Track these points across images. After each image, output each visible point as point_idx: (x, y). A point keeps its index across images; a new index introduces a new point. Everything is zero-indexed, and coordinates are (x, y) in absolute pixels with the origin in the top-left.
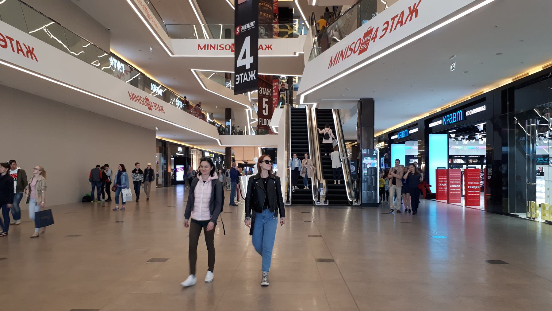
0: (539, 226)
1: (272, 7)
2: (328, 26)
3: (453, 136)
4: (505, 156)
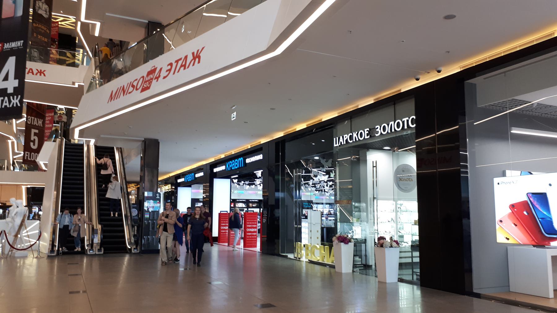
0: (304, 265)
1: (50, 30)
2: (110, 60)
3: (235, 181)
4: (277, 200)
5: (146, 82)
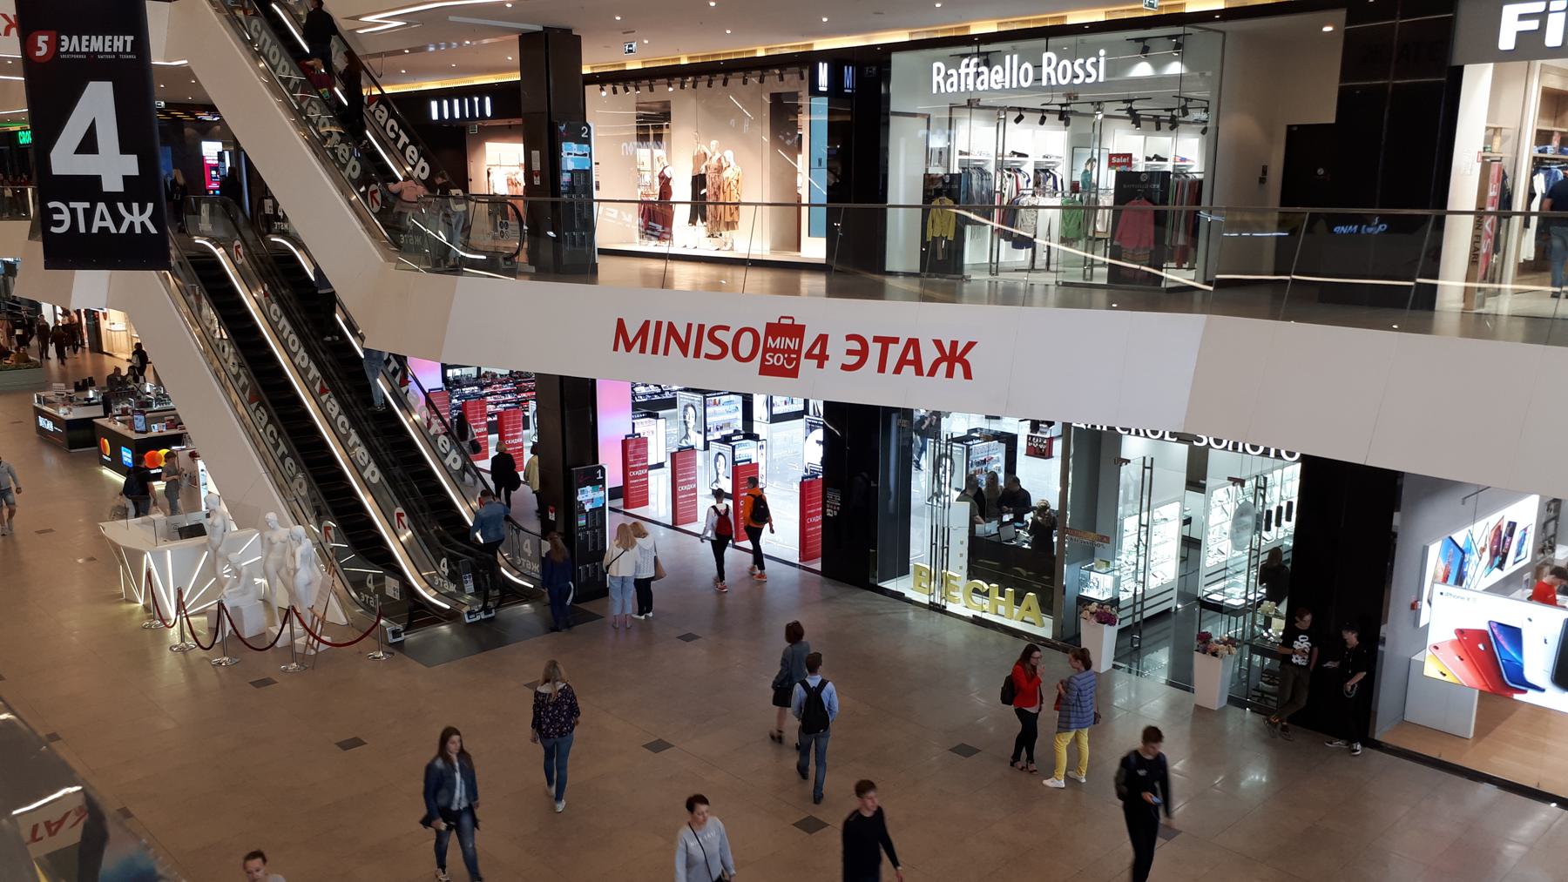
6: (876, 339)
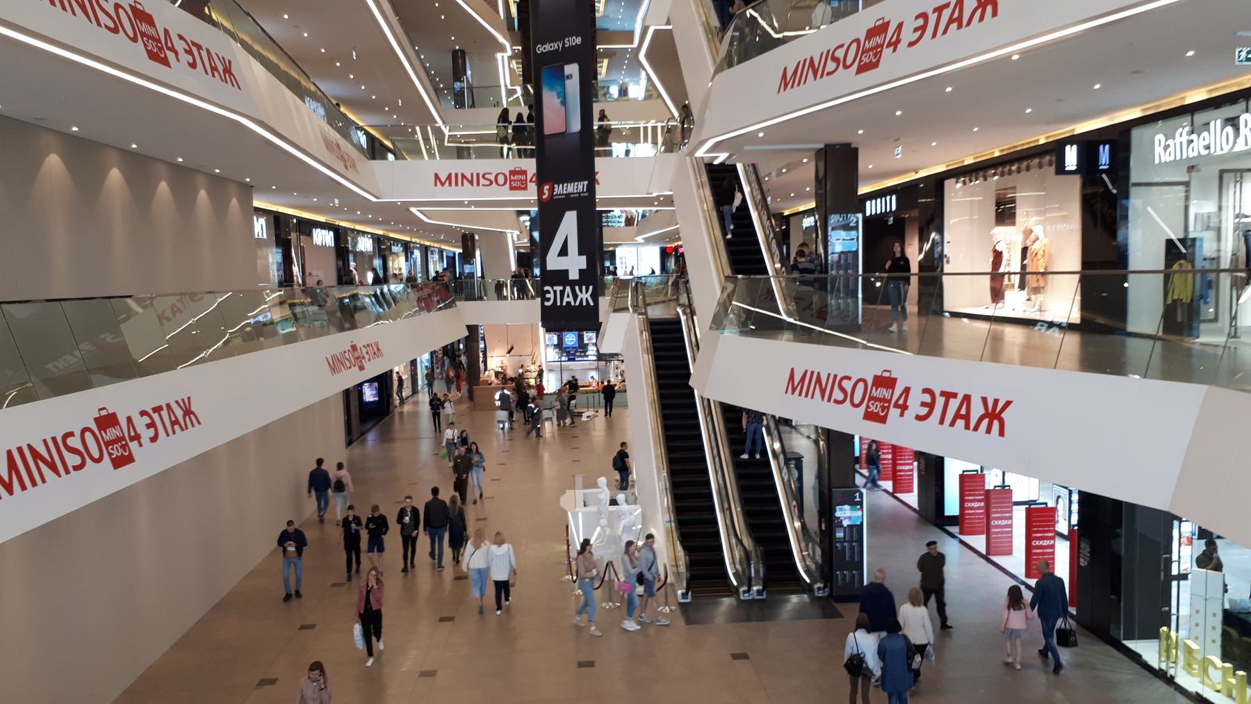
5: (865, 51)
6: (943, 394)
